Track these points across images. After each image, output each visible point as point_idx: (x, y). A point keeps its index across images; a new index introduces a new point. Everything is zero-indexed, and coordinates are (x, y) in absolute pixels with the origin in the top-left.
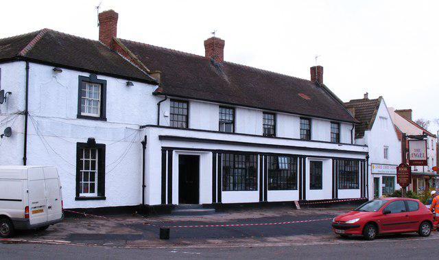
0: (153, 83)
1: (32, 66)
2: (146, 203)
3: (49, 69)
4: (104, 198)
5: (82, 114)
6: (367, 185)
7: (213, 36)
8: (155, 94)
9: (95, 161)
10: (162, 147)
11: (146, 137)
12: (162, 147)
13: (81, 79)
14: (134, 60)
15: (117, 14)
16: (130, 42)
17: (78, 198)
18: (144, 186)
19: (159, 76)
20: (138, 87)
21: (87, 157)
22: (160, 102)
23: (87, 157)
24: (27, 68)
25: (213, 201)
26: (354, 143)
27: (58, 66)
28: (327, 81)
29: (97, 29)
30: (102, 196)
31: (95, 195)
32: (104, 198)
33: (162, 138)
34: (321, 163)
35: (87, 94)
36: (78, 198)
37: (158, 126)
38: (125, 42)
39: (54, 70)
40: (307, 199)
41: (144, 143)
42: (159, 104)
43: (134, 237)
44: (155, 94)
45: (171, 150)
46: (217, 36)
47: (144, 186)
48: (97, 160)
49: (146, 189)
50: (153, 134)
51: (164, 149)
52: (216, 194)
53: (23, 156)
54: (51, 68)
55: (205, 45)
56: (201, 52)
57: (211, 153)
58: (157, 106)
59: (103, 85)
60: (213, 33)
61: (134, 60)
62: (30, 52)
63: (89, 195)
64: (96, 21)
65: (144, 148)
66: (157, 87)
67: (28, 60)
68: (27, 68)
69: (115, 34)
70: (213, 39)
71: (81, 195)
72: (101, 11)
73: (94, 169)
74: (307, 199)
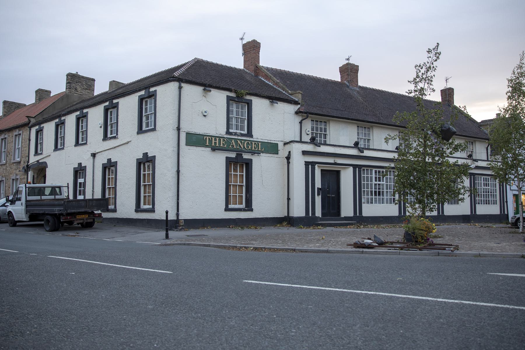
0: (296, 103)
1: (186, 87)
2: (291, 215)
3: (200, 89)
4: (252, 210)
5: (231, 131)
6: (507, 202)
7: (347, 62)
8: (297, 113)
9: (243, 175)
10: (305, 162)
11: (290, 152)
12: (305, 162)
13: (229, 99)
14: (276, 84)
15: (259, 44)
16: (272, 69)
17: (227, 209)
18: (289, 199)
19: (300, 96)
20: (281, 106)
21: (235, 170)
22: (302, 120)
23: (235, 170)
24: (180, 88)
25: (399, 214)
26: (489, 159)
27: (207, 86)
28: (458, 102)
29: (242, 59)
30: (249, 207)
31: (243, 206)
32: (252, 210)
33: (305, 153)
34: (338, 173)
35: (235, 113)
36: (227, 209)
37: (301, 142)
38: (267, 69)
39: (204, 90)
40: (478, 213)
41: (288, 158)
42: (301, 123)
43: (75, 236)
44: (297, 113)
45: (313, 164)
46: (351, 61)
47: (289, 199)
48: (244, 174)
49: (291, 202)
50: (297, 149)
51: (307, 164)
52: (358, 204)
53: (176, 169)
54: (202, 88)
55: (340, 72)
56: (337, 78)
57: (351, 169)
58: (299, 124)
59: (249, 104)
60: (348, 59)
61: (276, 84)
62: (183, 74)
63: (237, 206)
64: (240, 51)
65: (288, 163)
66: (299, 106)
67: (179, 80)
68: (180, 88)
69: (259, 62)
70: (348, 64)
71: (231, 206)
72: (245, 42)
73: (374, 191)
74: (478, 213)
